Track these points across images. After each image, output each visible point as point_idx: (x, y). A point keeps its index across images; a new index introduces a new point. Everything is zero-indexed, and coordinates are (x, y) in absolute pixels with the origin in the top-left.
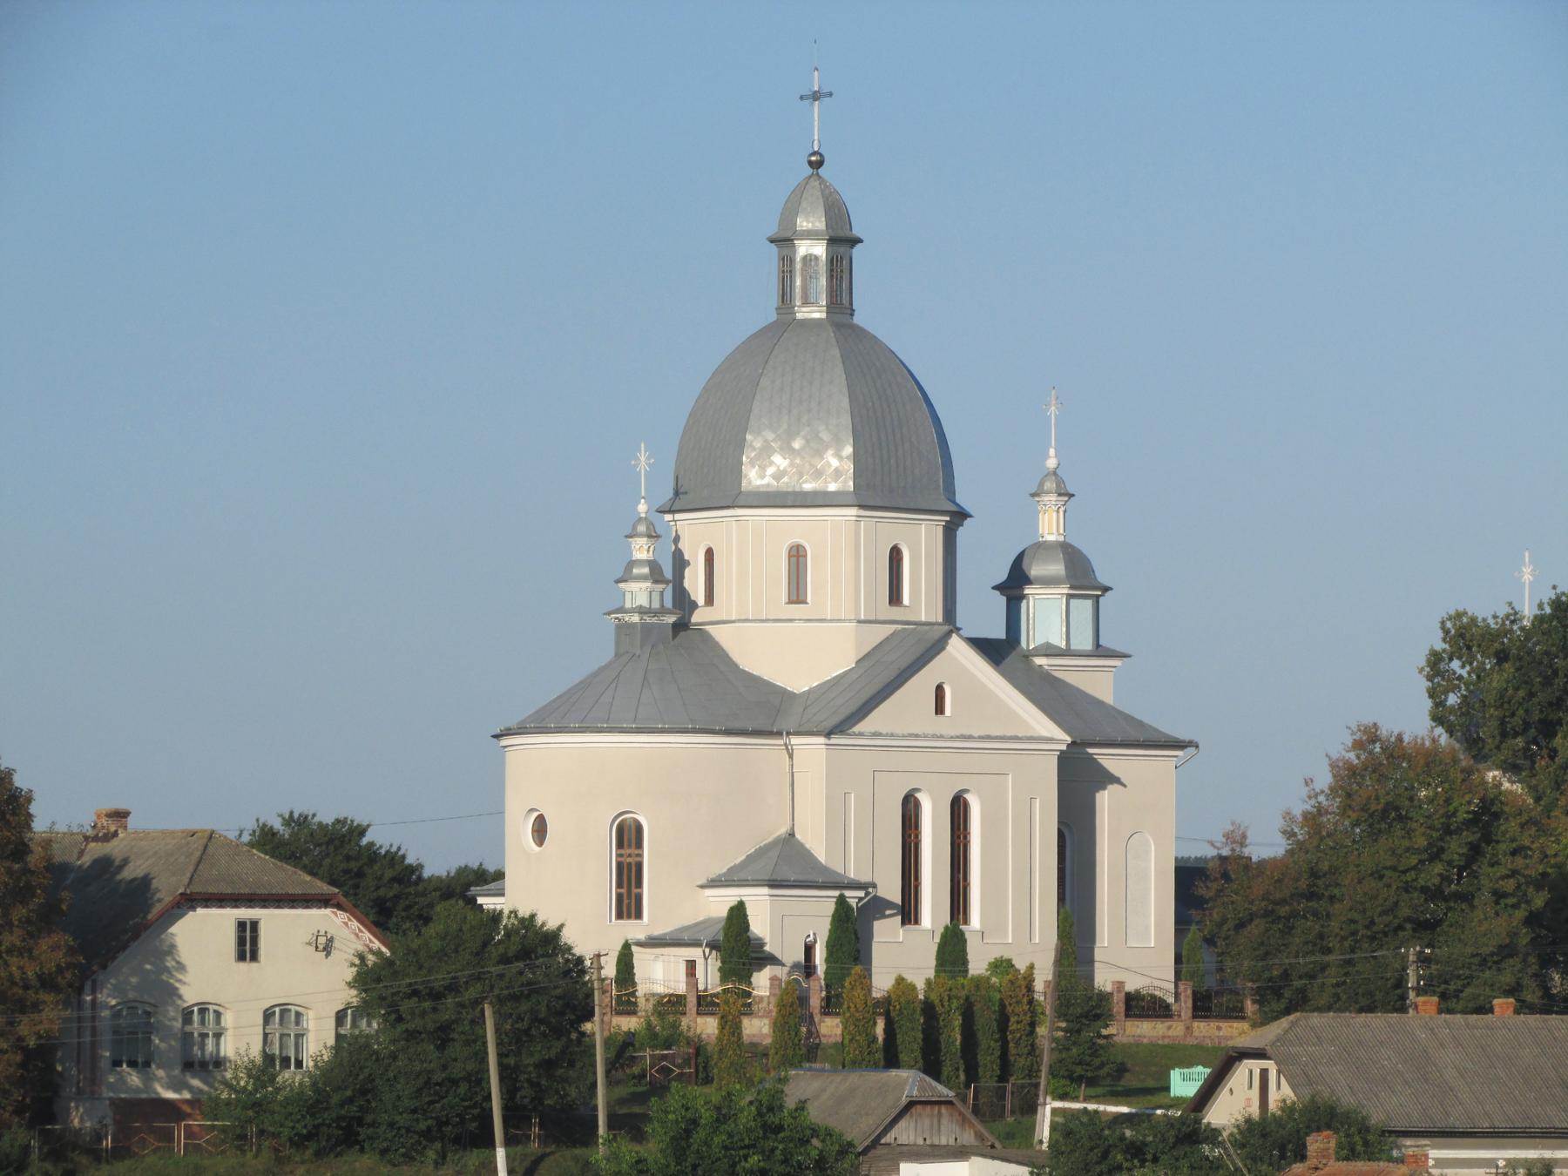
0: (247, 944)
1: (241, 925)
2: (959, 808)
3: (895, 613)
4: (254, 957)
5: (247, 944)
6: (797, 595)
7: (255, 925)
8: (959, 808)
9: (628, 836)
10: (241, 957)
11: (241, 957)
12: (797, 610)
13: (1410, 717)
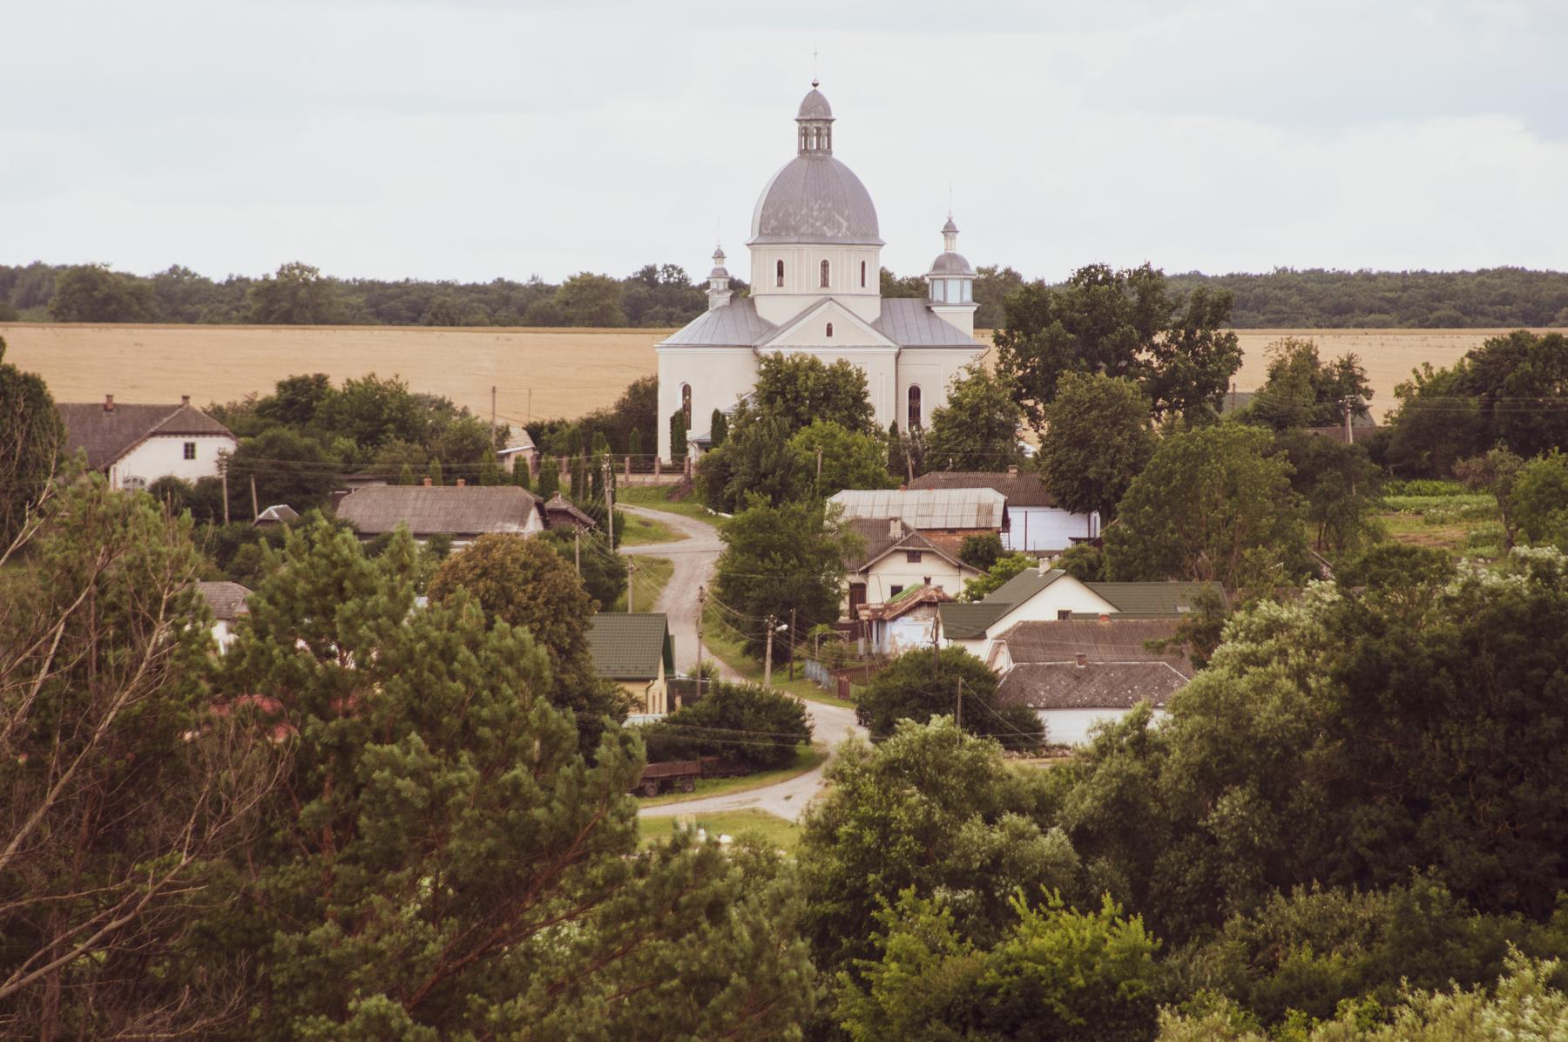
0: (190, 452)
1: (187, 445)
4: (193, 457)
5: (190, 452)
7: (193, 445)
10: (186, 457)
11: (186, 457)
12: (780, 290)
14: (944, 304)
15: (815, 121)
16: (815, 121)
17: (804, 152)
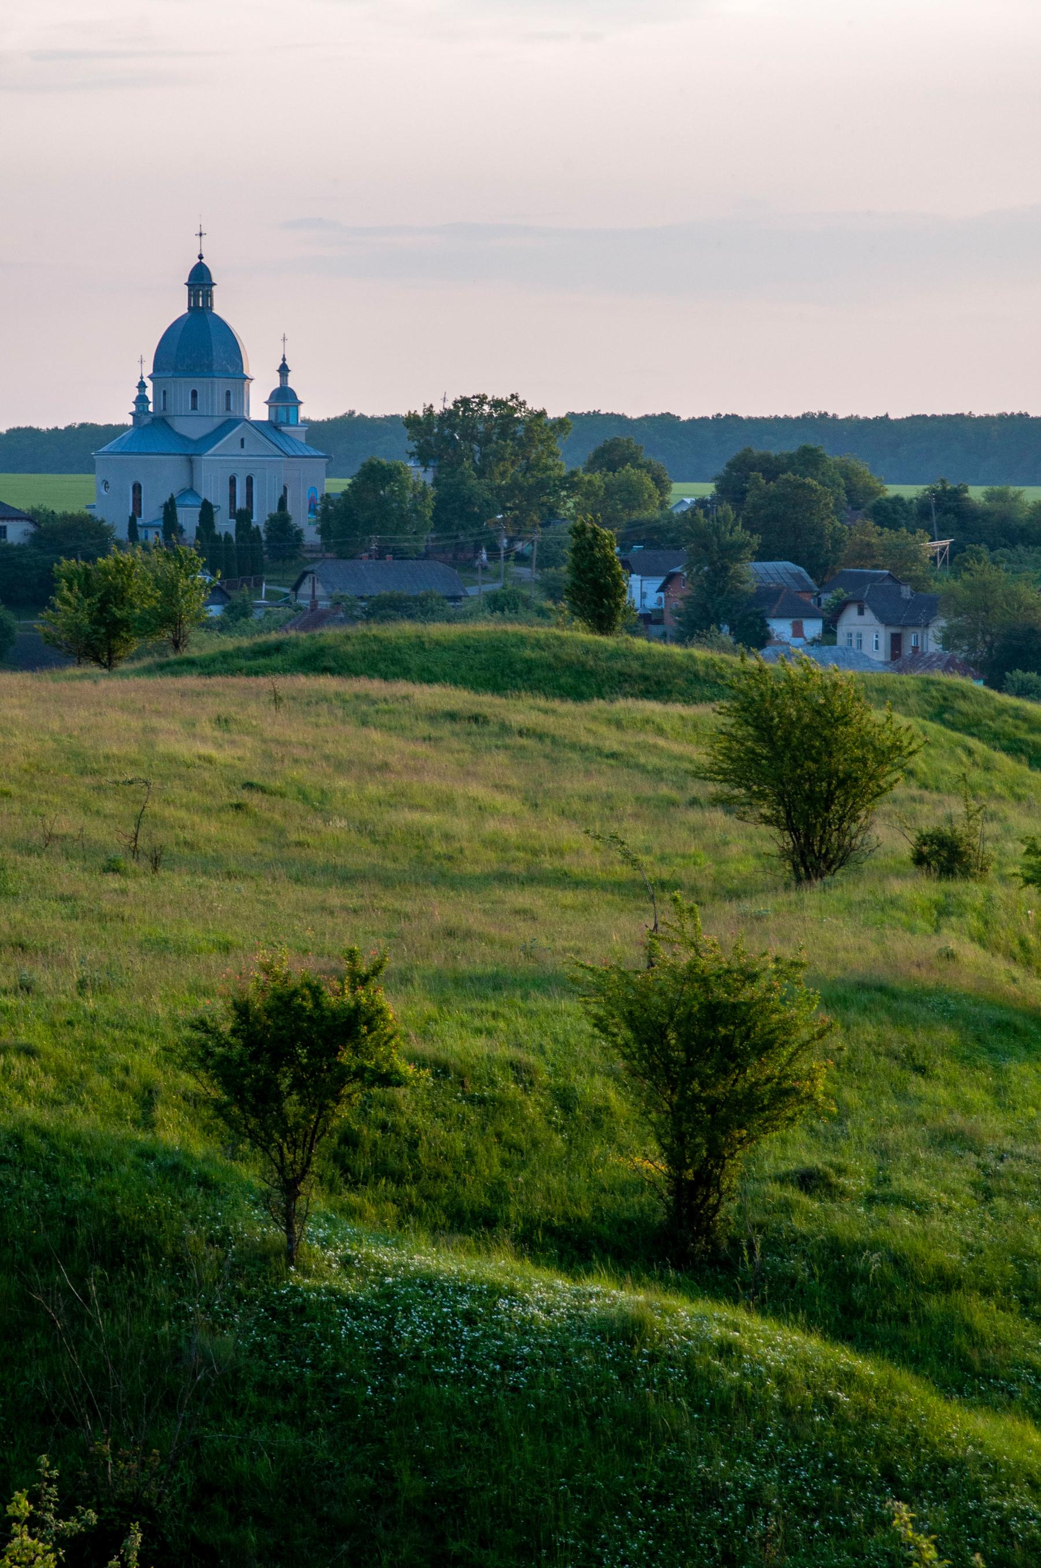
2: (249, 481)
3: (228, 413)
6: (194, 407)
8: (249, 481)
9: (137, 488)
12: (195, 413)
13: (830, 414)
14: (288, 424)
15: (200, 280)
16: (200, 280)
17: (190, 308)
